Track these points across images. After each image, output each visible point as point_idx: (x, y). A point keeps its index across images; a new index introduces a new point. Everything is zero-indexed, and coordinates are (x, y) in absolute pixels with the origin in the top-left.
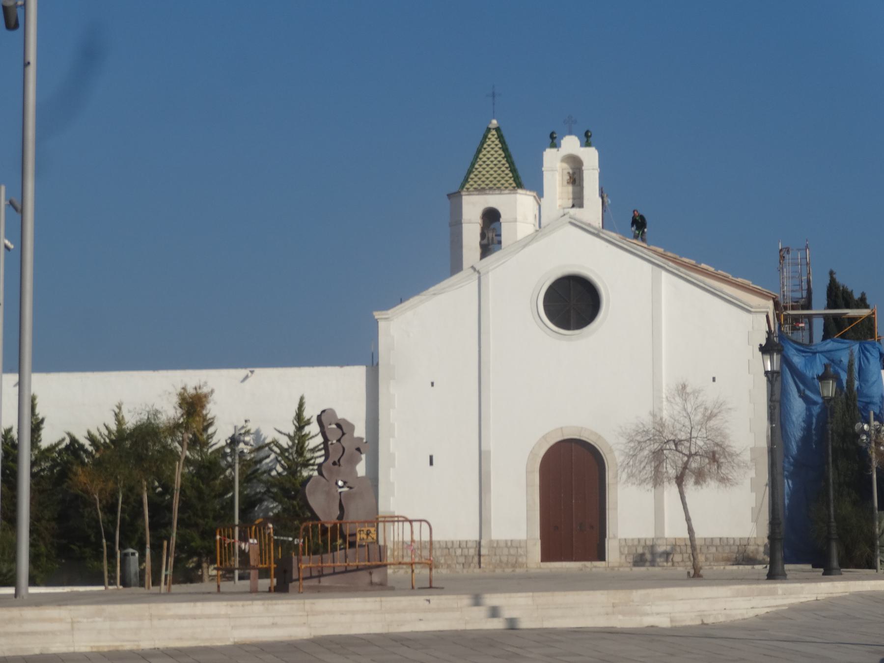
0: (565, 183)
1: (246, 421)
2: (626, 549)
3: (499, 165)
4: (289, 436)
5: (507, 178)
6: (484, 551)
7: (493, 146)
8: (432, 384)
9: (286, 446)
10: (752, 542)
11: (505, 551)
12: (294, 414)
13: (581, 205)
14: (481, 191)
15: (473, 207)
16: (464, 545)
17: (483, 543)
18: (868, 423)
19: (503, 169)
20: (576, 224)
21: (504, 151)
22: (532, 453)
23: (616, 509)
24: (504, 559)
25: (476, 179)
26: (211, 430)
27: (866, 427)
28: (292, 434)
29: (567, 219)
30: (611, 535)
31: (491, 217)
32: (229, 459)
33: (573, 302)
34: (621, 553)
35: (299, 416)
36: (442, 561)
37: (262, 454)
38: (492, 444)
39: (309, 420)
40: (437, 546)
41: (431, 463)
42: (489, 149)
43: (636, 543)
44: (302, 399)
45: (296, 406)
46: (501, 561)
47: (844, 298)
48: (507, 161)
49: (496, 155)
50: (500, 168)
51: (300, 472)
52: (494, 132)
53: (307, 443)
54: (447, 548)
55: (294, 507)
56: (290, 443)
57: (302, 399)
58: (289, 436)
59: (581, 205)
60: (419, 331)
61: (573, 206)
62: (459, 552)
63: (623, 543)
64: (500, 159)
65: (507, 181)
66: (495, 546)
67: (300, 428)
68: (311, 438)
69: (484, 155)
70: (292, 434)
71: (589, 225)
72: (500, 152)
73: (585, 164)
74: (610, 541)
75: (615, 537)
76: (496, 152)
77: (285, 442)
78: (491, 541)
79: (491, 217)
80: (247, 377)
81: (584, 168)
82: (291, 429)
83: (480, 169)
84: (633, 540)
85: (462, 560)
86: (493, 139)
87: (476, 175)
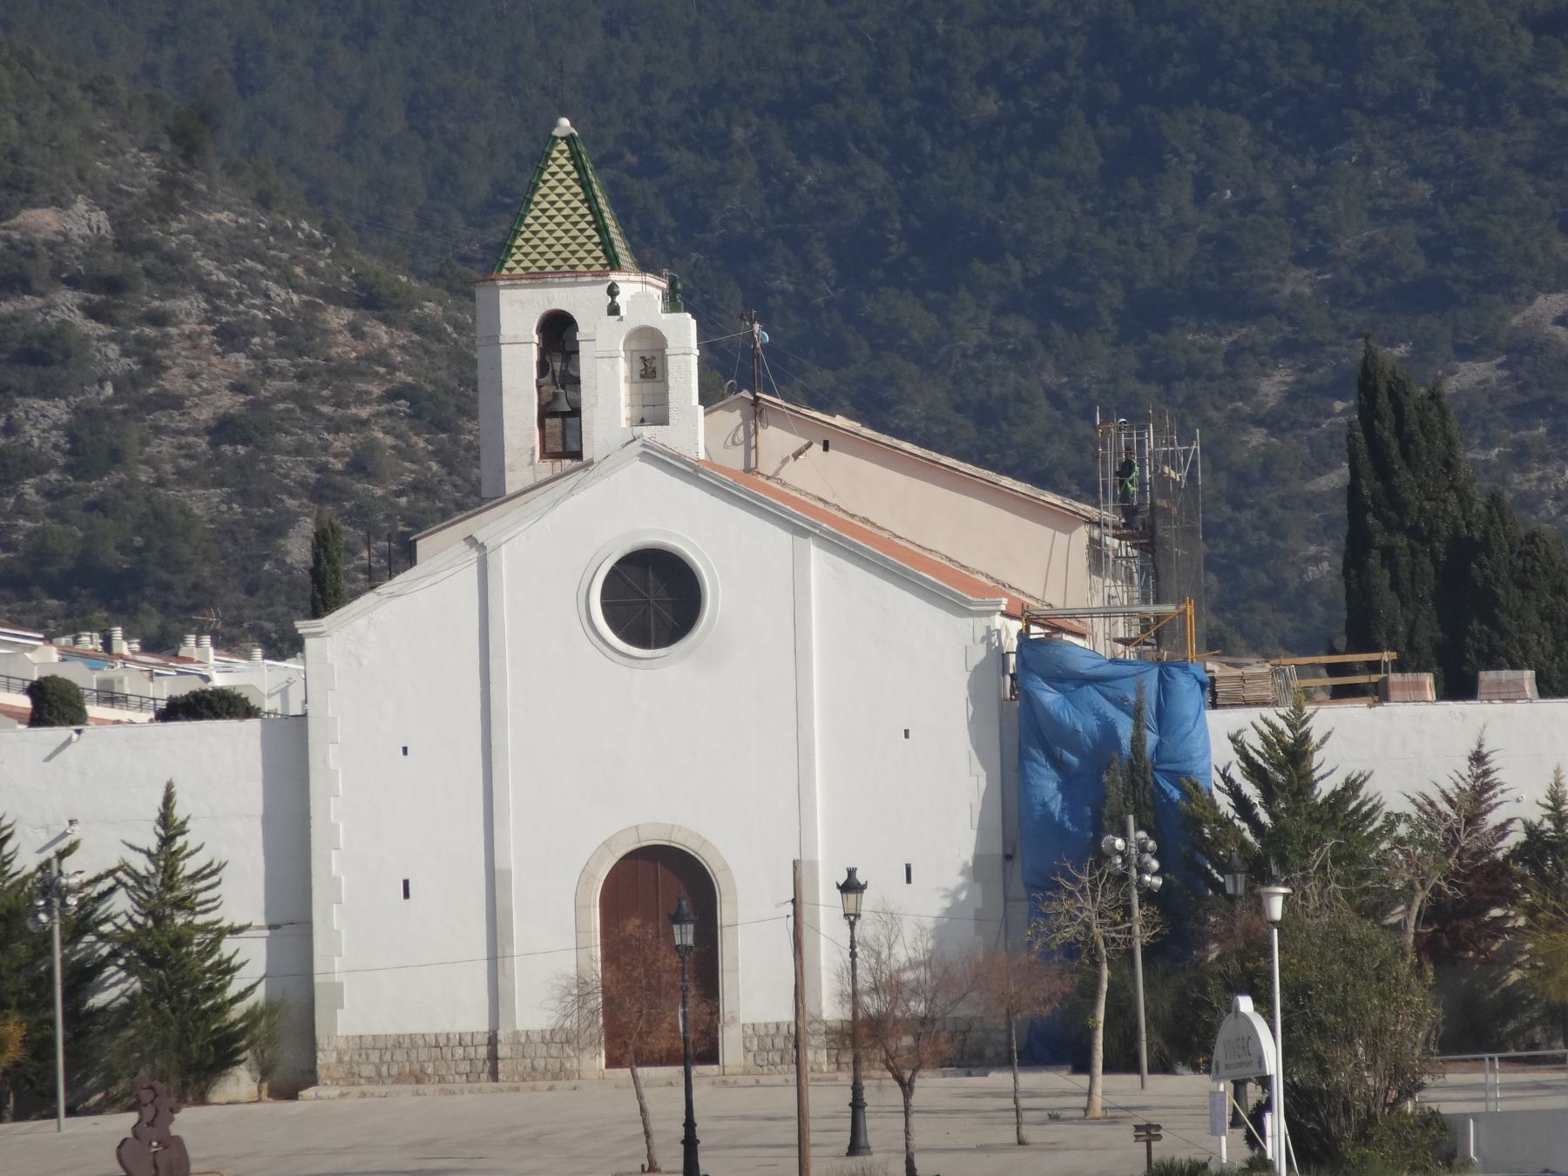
0: (637, 377)
1: (71, 822)
2: (755, 1041)
3: (575, 218)
4: (149, 854)
5: (590, 246)
6: (503, 1051)
7: (561, 175)
8: (405, 750)
9: (144, 873)
10: (977, 1024)
11: (542, 1050)
12: (157, 815)
13: (664, 421)
14: (537, 277)
15: (518, 313)
16: (468, 1040)
17: (501, 1035)
18: (1124, 834)
19: (583, 225)
20: (658, 458)
21: (582, 187)
22: (586, 874)
23: (736, 970)
24: (540, 1063)
25: (527, 249)
26: (8, 848)
27: (1119, 843)
28: (154, 850)
29: (636, 448)
30: (728, 1017)
31: (558, 333)
32: (43, 917)
33: (653, 598)
34: (747, 1050)
35: (165, 819)
36: (430, 1070)
37: (89, 908)
38: (511, 857)
39: (184, 823)
40: (421, 1043)
41: (406, 895)
42: (553, 183)
43: (772, 1031)
44: (169, 786)
45: (159, 801)
46: (534, 1069)
47: (1391, 393)
48: (589, 208)
49: (567, 197)
50: (575, 224)
51: (171, 917)
52: (563, 146)
53: (181, 864)
54: (437, 1046)
55: (160, 979)
56: (152, 869)
57: (169, 786)
58: (149, 854)
59: (664, 421)
60: (377, 661)
61: (642, 421)
62: (460, 1052)
63: (750, 1032)
64: (576, 204)
65: (589, 252)
66: (523, 1041)
67: (167, 841)
68: (188, 855)
69: (544, 196)
70: (154, 850)
71: (679, 458)
72: (577, 189)
73: (669, 343)
74: (726, 1030)
75: (734, 1019)
76: (568, 188)
77: (141, 864)
78: (516, 1034)
79: (558, 333)
80: (69, 741)
81: (668, 352)
82: (153, 843)
83: (536, 227)
84: (766, 1025)
85: (465, 1067)
86: (562, 161)
87: (527, 240)
